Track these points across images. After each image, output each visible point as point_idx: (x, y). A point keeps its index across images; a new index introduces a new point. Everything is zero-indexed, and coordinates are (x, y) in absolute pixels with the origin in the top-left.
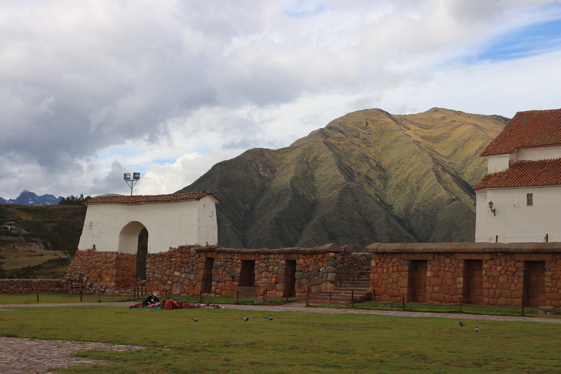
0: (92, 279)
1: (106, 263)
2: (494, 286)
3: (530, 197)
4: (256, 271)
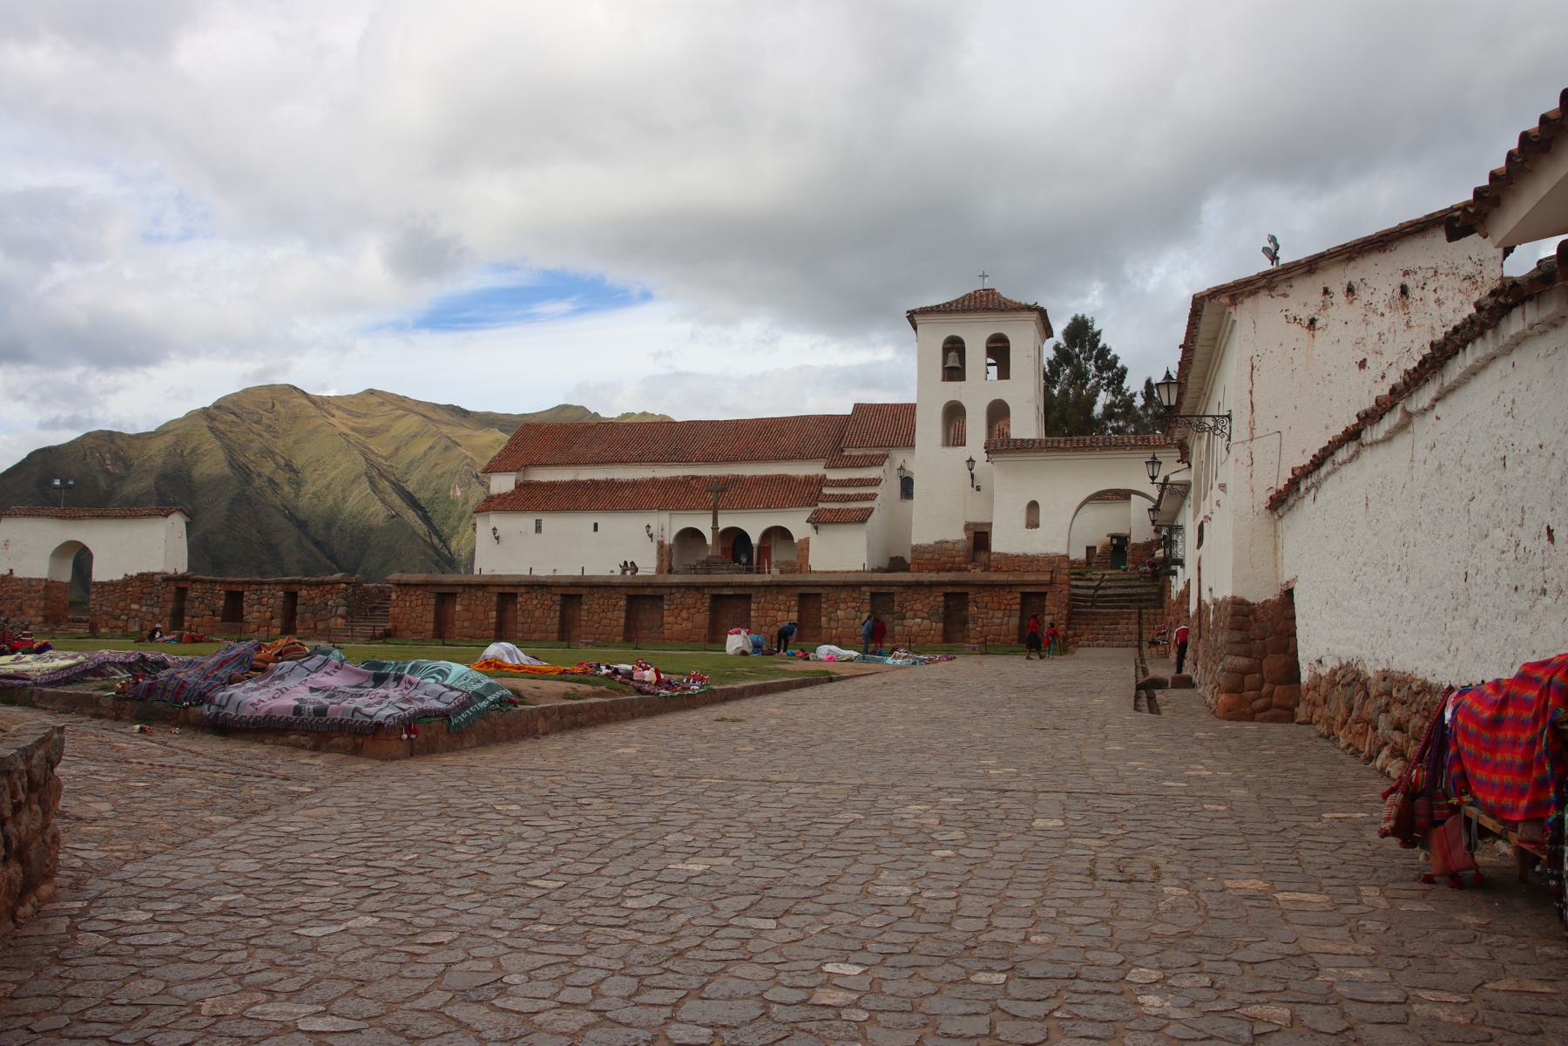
0: (7, 613)
1: (29, 592)
2: (529, 620)
4: (244, 604)
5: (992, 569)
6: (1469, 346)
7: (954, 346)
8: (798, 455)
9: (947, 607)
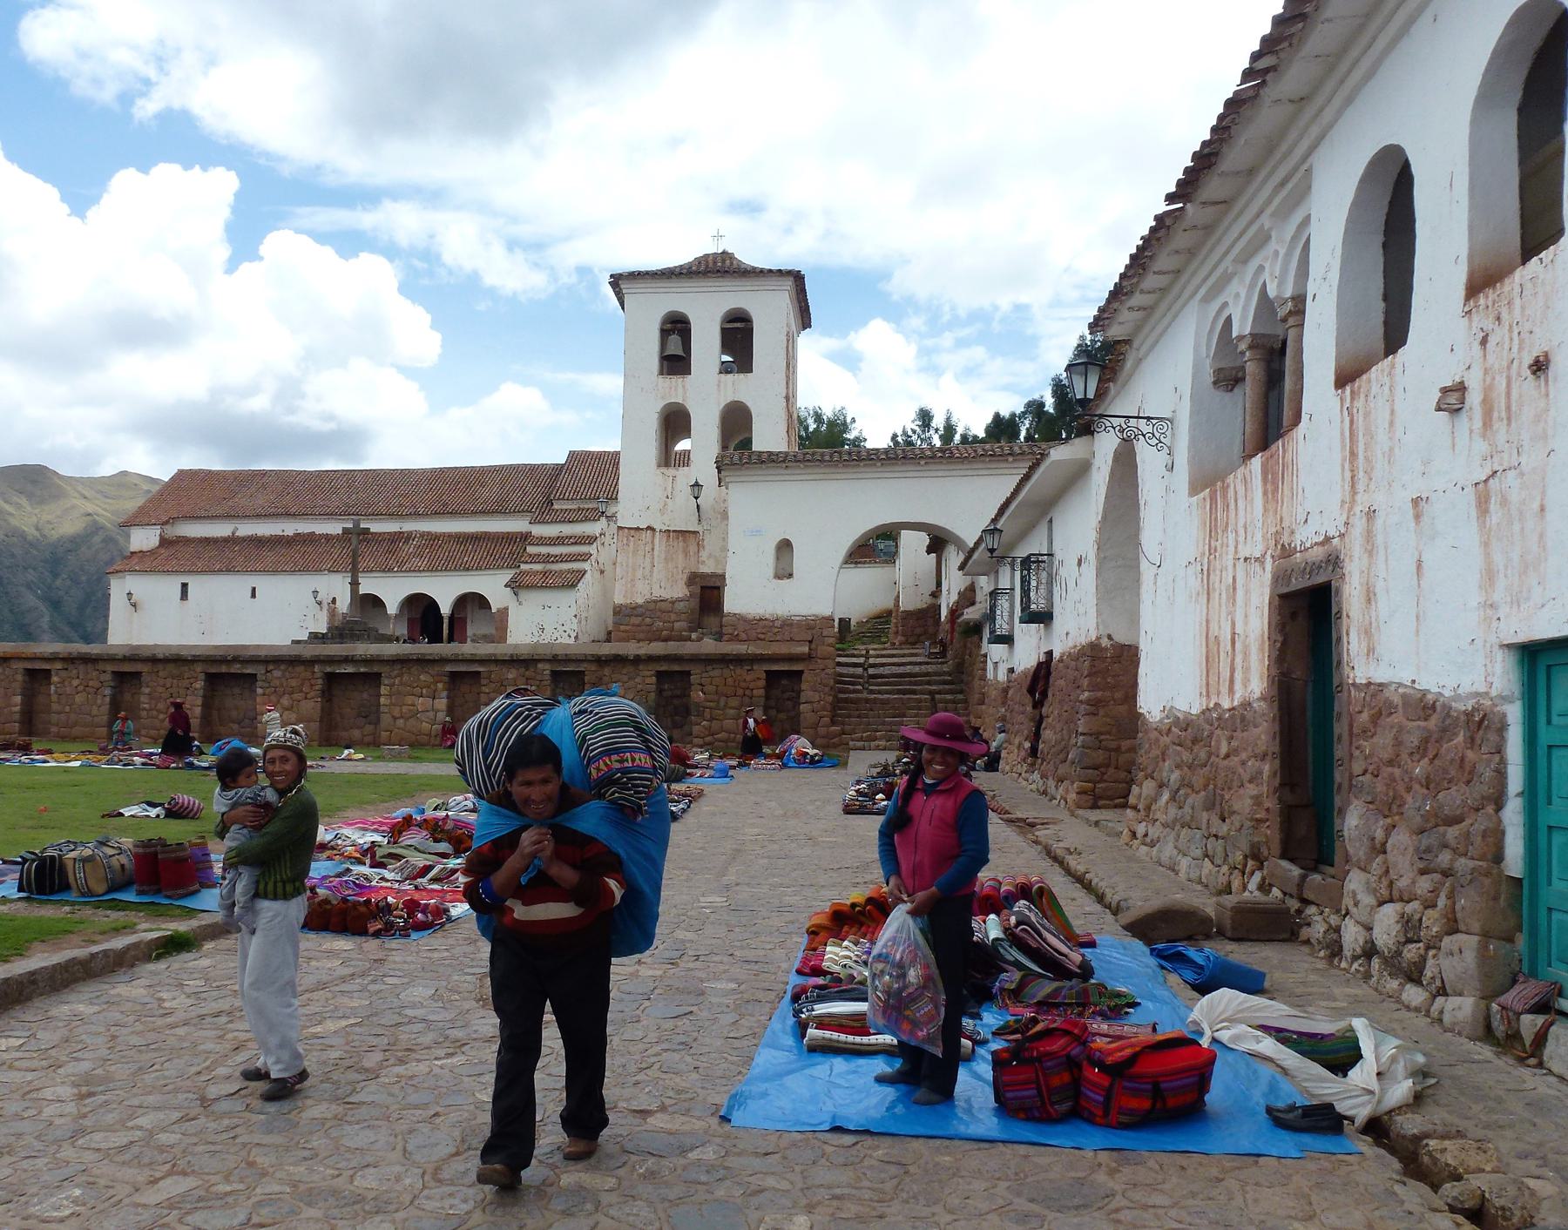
3: (185, 586)
5: (725, 638)
6: (1498, 285)
7: (677, 326)
9: (660, 692)
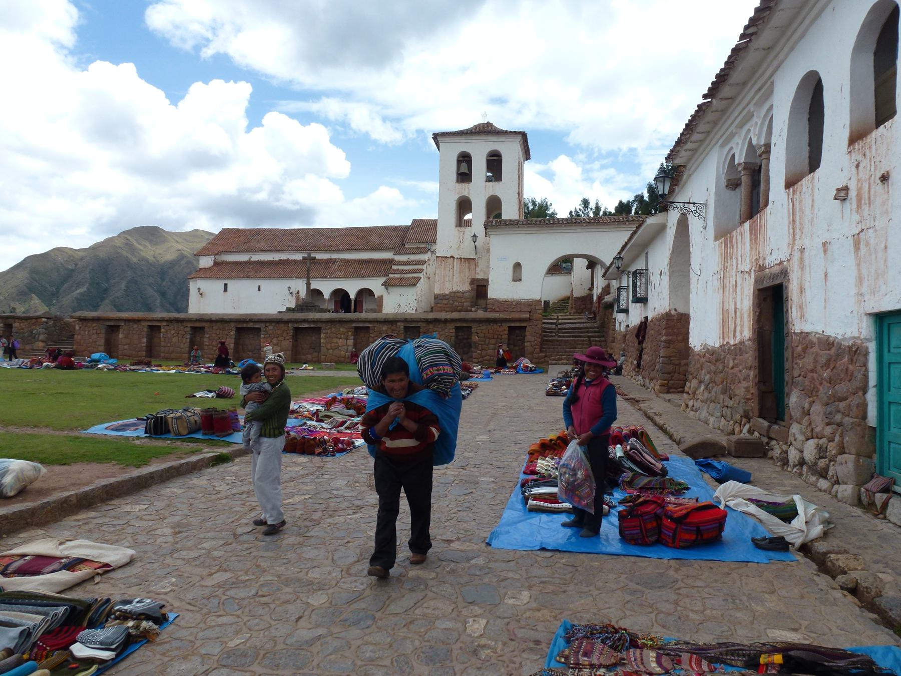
7: (465, 159)
8: (378, 248)
9: (457, 337)
